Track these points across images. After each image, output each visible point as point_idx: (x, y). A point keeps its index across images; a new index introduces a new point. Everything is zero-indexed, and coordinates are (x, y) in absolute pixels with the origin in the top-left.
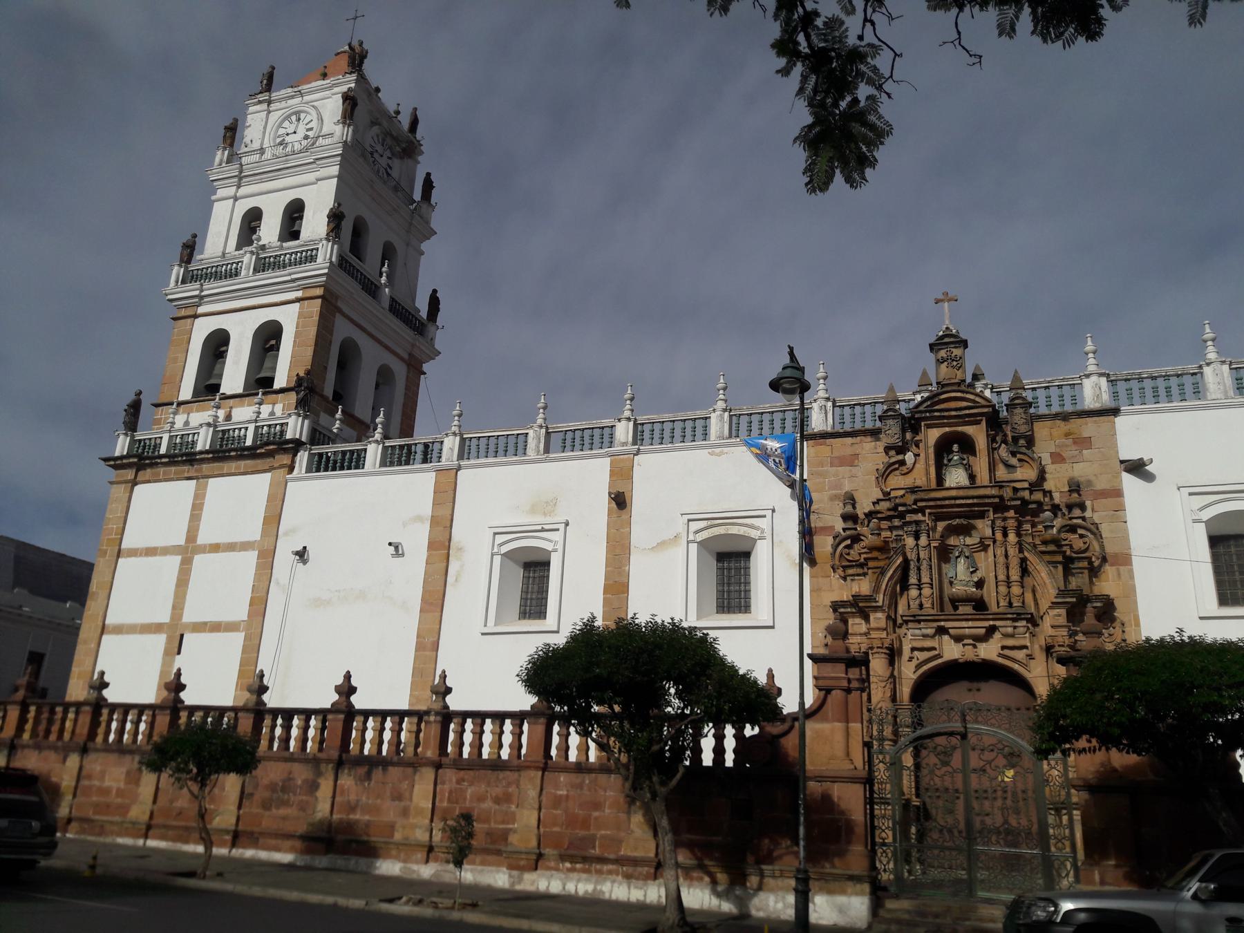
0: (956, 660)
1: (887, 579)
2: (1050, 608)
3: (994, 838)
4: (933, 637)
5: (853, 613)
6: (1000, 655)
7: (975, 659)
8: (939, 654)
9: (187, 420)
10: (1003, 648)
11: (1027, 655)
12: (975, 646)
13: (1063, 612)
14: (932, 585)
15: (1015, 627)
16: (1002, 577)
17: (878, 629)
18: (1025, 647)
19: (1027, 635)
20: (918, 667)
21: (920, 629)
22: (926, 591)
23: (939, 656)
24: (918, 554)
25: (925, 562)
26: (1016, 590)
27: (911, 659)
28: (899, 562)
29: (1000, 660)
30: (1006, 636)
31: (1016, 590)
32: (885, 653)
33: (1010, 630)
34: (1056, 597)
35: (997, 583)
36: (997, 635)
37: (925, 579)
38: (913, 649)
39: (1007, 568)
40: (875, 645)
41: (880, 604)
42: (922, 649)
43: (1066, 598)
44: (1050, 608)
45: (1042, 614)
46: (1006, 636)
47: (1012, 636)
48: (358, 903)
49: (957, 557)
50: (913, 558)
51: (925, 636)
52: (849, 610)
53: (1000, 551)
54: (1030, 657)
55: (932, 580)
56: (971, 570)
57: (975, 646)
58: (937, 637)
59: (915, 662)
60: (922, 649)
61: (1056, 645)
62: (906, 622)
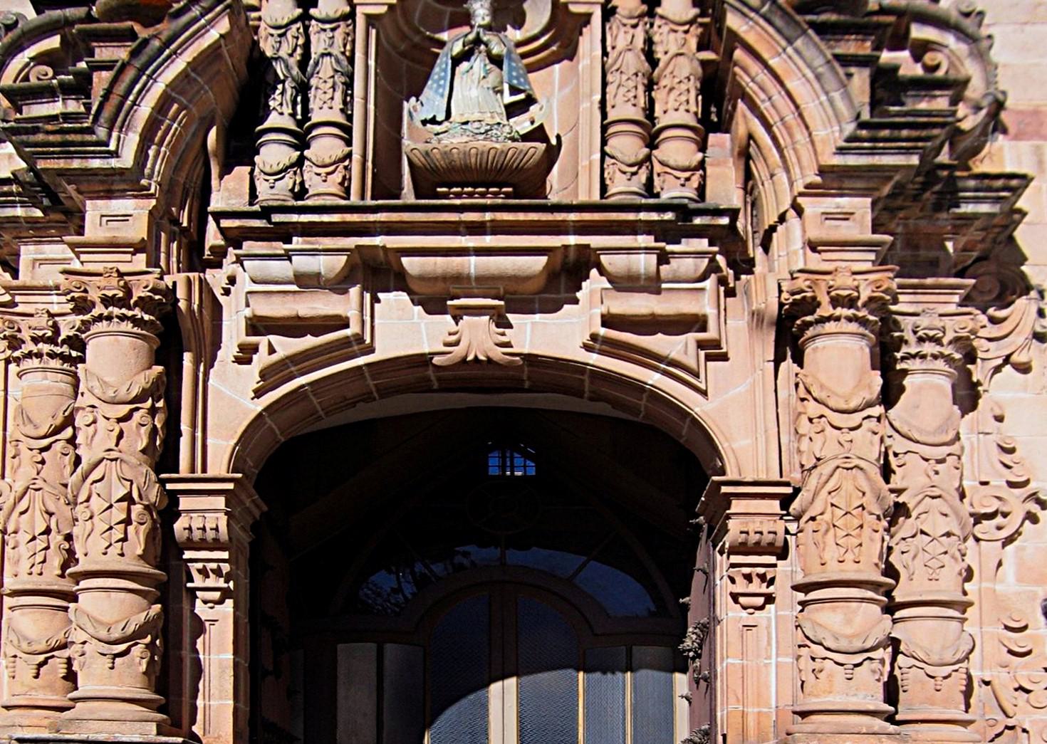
0: (423, 360)
1: (158, 89)
2: (812, 190)
3: (378, 230)
4: (339, 285)
5: (32, 221)
6: (595, 344)
7: (498, 354)
8: (359, 338)
9: (892, 676)
10: (608, 321)
11: (701, 345)
12: (504, 324)
13: (861, 206)
14: (348, 130)
15: (663, 258)
16: (625, 107)
17: (113, 246)
18: (696, 323)
19: (709, 284)
20: (271, 377)
21: (287, 256)
22: (325, 147)
23: (360, 345)
24: (307, 46)
25: (327, 67)
26: (676, 150)
27: (246, 355)
28: (213, 35)
29: (594, 359)
30: (625, 283)
31: (676, 150)
32: (136, 321)
33: (644, 263)
34: (841, 151)
35: (604, 128)
36: (594, 283)
37: (324, 108)
38: (257, 326)
39: (650, 86)
40: (94, 295)
41: (152, 191)
42: (293, 327)
43: (884, 152)
44: (812, 190)
45: (770, 218)
46: (625, 283)
47: (652, 285)
48: (707, 488)
49: (456, 61)
50: (283, 53)
51: (307, 282)
52: (19, 212)
53: (626, 38)
54: (714, 351)
55: (350, 118)
56: (508, 99)
57: (504, 324)
58: (354, 291)
59: (262, 359)
60: (293, 327)
61: (824, 299)
62: (234, 239)
